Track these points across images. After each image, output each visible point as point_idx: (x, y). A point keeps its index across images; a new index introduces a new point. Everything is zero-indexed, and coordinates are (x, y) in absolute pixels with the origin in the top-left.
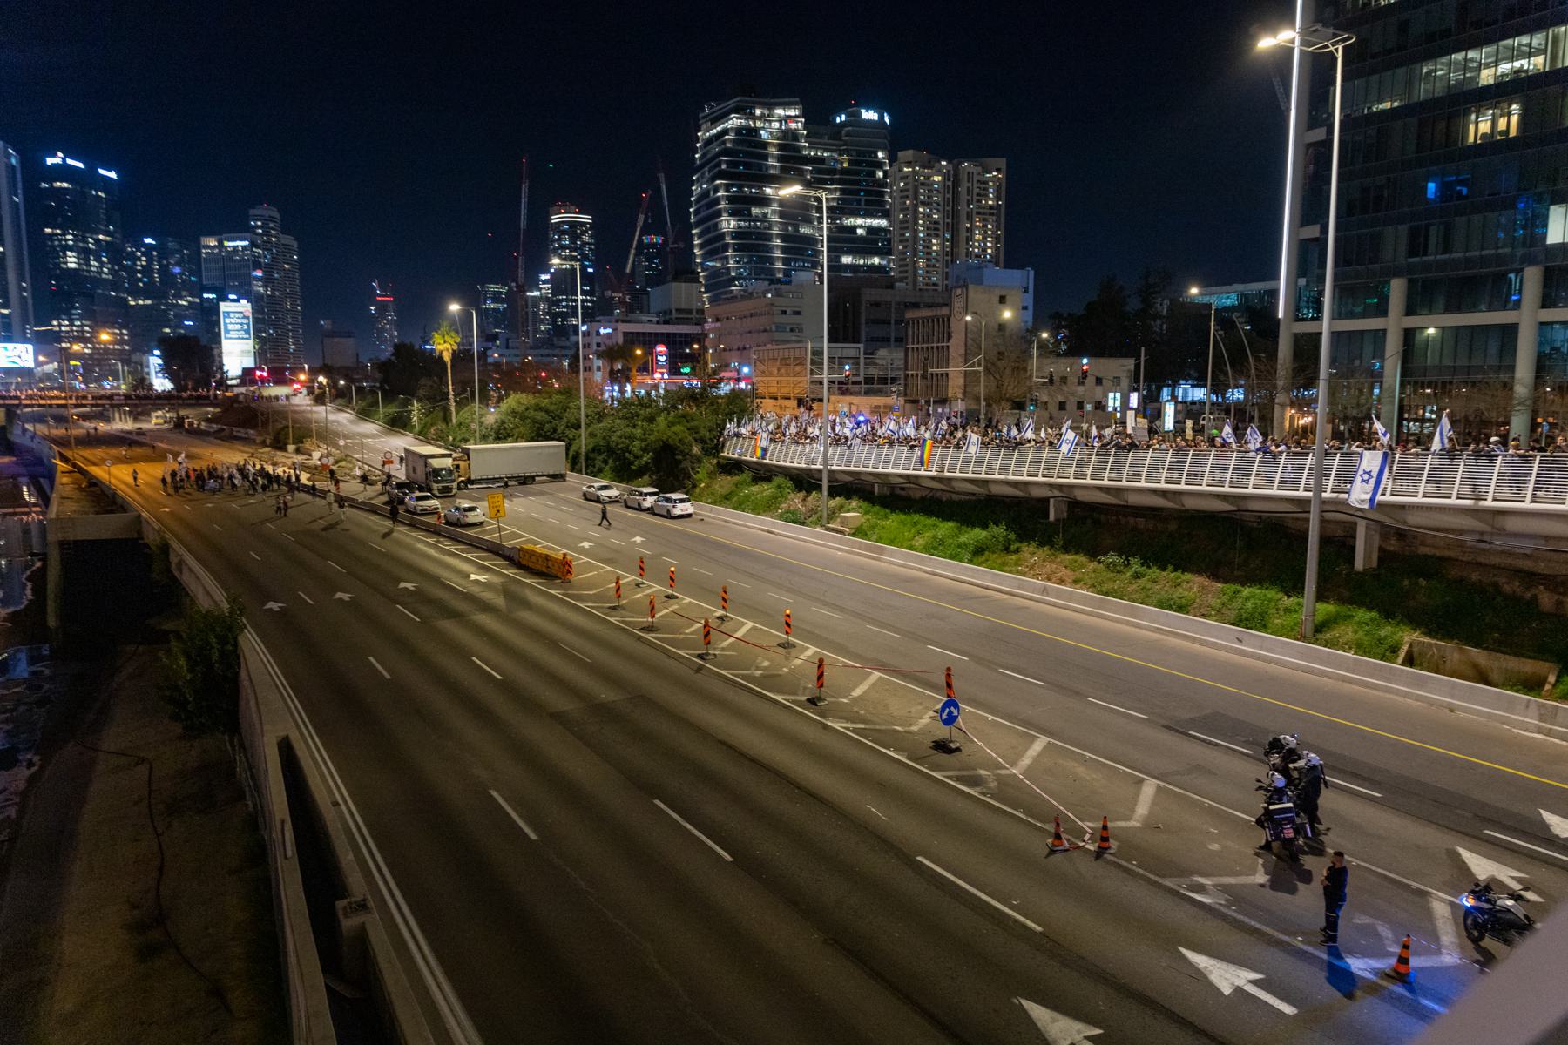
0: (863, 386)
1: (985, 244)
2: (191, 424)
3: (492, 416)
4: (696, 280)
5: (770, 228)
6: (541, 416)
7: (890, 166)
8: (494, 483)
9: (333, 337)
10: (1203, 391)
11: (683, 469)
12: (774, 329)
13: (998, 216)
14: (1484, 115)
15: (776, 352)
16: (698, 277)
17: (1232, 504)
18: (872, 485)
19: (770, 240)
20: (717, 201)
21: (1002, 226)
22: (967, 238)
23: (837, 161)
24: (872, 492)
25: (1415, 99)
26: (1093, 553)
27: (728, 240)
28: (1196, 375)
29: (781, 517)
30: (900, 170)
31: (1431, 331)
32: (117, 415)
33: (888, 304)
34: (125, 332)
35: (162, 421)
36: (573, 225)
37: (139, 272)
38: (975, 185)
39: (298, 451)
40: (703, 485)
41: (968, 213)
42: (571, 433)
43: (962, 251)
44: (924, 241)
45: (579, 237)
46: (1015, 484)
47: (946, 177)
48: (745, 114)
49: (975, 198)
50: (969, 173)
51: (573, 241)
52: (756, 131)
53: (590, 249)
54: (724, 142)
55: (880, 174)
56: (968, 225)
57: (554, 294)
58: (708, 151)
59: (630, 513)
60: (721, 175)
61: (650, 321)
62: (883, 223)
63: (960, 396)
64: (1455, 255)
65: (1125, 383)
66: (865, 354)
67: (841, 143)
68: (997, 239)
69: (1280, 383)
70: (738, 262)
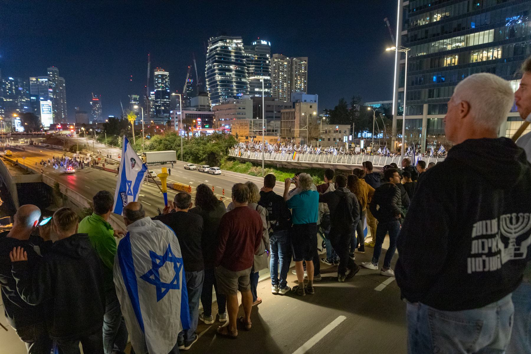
1: (301, 85)
2: (35, 144)
3: (148, 143)
4: (207, 96)
5: (232, 79)
6: (167, 142)
7: (271, 59)
8: (154, 164)
9: (80, 113)
10: (371, 134)
11: (218, 160)
13: (305, 76)
14: (449, 58)
16: (208, 95)
17: (380, 170)
18: (277, 164)
19: (232, 83)
20: (214, 70)
21: (307, 79)
22: (295, 83)
23: (253, 57)
24: (276, 167)
25: (430, 53)
27: (218, 83)
28: (368, 129)
29: (249, 174)
30: (274, 60)
31: (436, 119)
32: (7, 140)
33: (273, 106)
34: (3, 110)
35: (24, 142)
36: (162, 75)
37: (8, 89)
38: (298, 66)
39: (80, 153)
40: (223, 164)
42: (177, 148)
43: (294, 88)
44: (281, 84)
45: (164, 79)
46: (320, 164)
47: (288, 63)
48: (224, 41)
50: (296, 62)
51: (162, 81)
52: (227, 47)
53: (168, 84)
54: (217, 51)
55: (267, 62)
56: (296, 79)
57: (156, 99)
58: (211, 53)
59: (201, 173)
60: (216, 61)
61: (193, 110)
62: (268, 78)
63: (298, 136)
64: (440, 98)
65: (348, 133)
66: (267, 122)
68: (305, 83)
69: (393, 134)
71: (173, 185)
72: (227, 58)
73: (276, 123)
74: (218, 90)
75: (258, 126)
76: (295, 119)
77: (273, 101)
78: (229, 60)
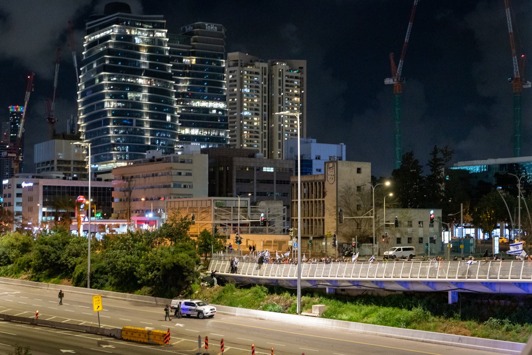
0: (250, 227)
12: (172, 186)
15: (177, 204)
20: (102, 87)
26: (482, 319)
27: (109, 115)
40: (197, 292)
41: (280, 98)
49: (285, 88)
54: (107, 45)
60: (105, 68)
61: (58, 177)
67: (191, 46)
70: (116, 133)
71: (121, 330)
72: (131, 61)
73: (271, 205)
74: (108, 133)
75: (232, 213)
76: (324, 197)
77: (253, 159)
78: (135, 65)
